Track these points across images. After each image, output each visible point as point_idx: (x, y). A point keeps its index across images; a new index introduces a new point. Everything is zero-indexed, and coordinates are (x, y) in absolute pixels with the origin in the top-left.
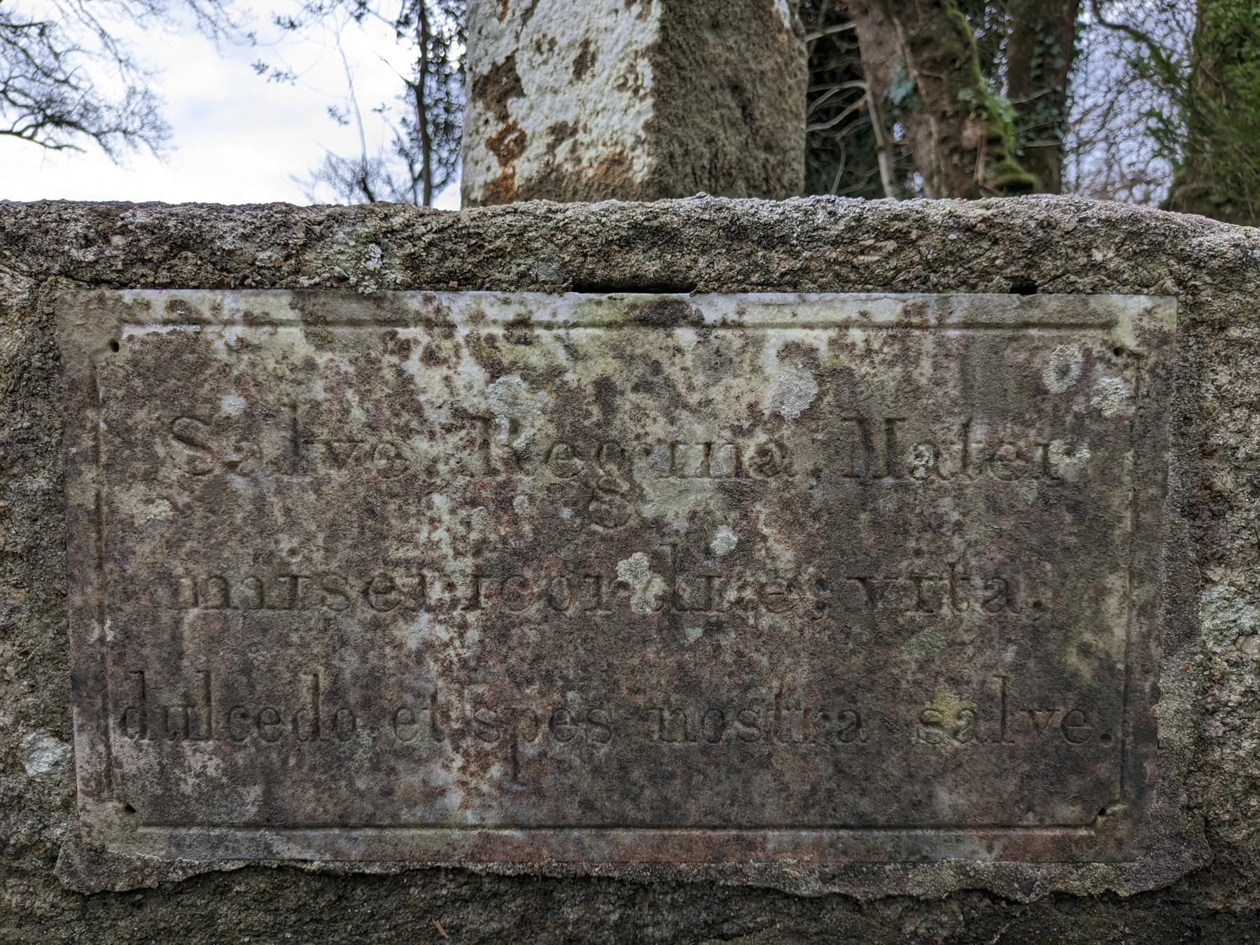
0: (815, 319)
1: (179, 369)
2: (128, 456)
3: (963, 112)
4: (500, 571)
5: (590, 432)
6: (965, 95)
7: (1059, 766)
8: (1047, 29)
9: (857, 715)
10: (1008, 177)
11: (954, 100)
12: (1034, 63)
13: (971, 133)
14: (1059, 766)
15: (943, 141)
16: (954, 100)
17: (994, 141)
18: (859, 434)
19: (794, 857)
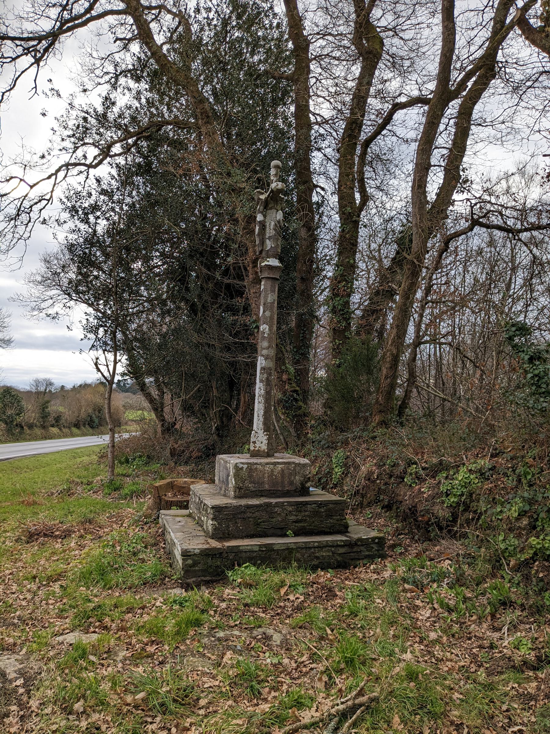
0: (281, 466)
1: (256, 468)
2: (254, 472)
3: (283, 372)
4: (269, 477)
5: (272, 471)
6: (283, 368)
7: (291, 484)
8: (304, 326)
9: (283, 482)
10: (293, 389)
11: (281, 369)
12: (301, 335)
13: (285, 377)
14: (291, 484)
15: (278, 378)
16: (281, 369)
17: (290, 379)
18: (283, 470)
19: (280, 489)
